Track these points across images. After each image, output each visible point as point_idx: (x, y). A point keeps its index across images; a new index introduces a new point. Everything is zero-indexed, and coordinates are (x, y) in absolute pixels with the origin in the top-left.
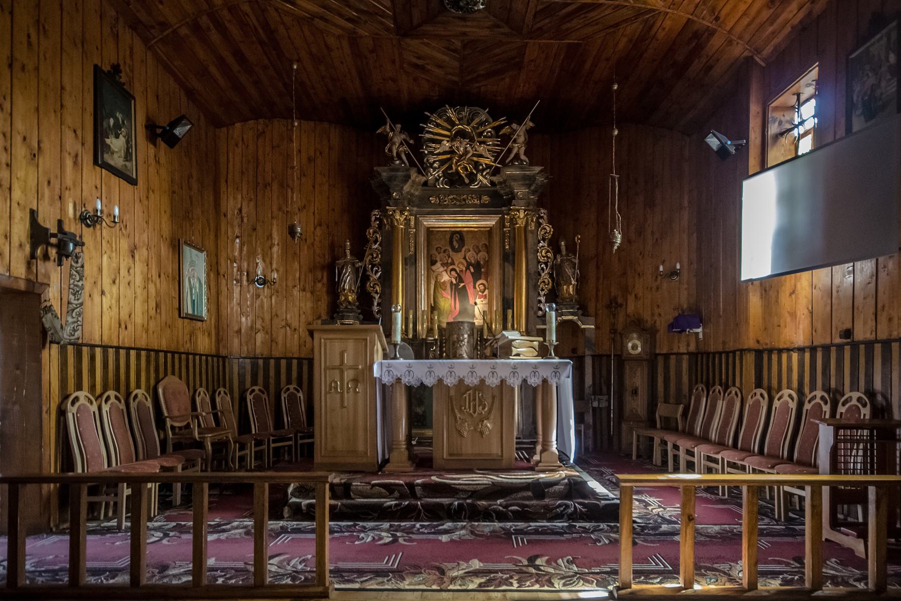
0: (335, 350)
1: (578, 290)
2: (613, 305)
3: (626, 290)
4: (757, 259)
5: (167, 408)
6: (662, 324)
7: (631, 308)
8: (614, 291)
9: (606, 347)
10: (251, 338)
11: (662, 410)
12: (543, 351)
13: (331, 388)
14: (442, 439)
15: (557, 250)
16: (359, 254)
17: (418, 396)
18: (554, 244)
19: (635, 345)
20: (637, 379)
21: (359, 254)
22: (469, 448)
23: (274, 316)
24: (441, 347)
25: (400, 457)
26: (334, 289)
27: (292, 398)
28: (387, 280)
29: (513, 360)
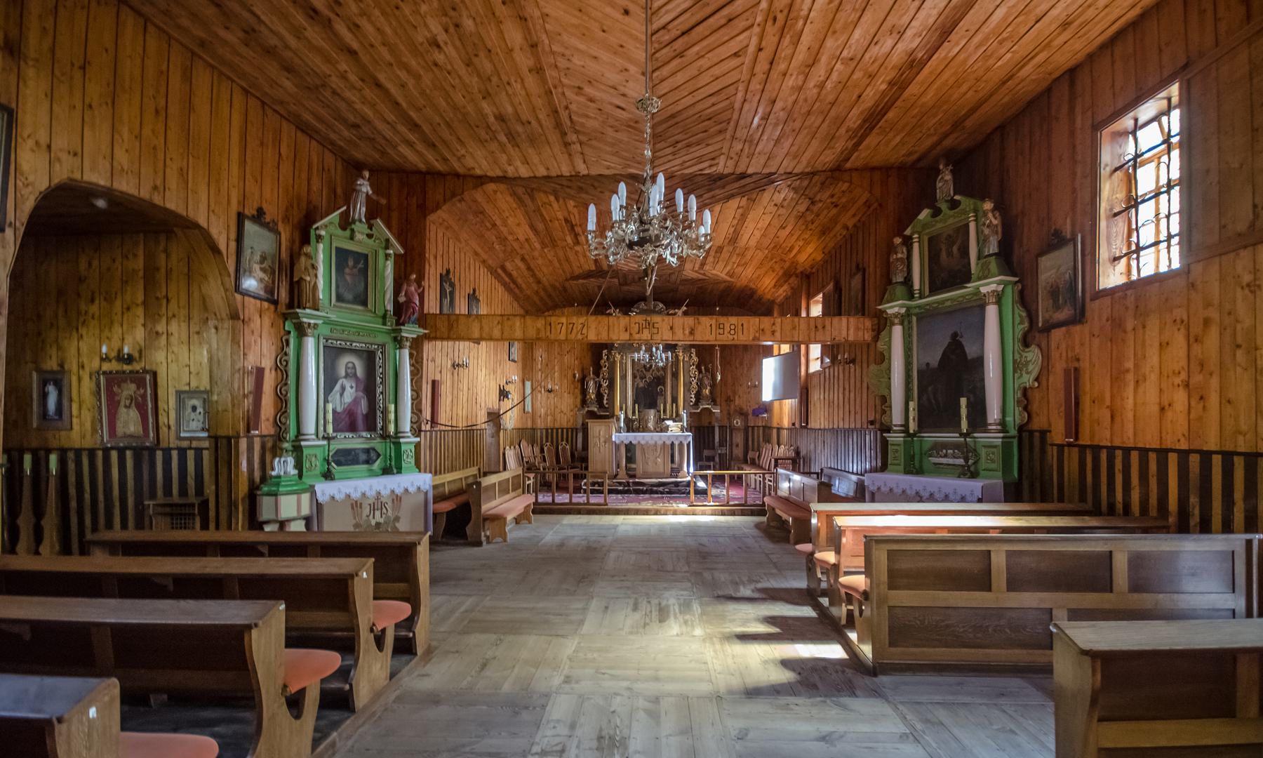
0: (596, 428)
1: (711, 392)
2: (729, 400)
3: (735, 393)
4: (767, 395)
5: (101, 412)
6: (750, 412)
7: (737, 402)
8: (730, 393)
9: (726, 423)
10: (546, 419)
11: (750, 455)
12: (682, 429)
13: (595, 445)
14: (639, 466)
15: (700, 372)
16: (597, 374)
17: (630, 448)
18: (698, 367)
19: (738, 422)
20: (739, 438)
21: (597, 374)
22: (651, 469)
23: (556, 407)
24: (619, 294)
25: (622, 472)
26: (584, 392)
27: (564, 449)
28: (611, 386)
29: (669, 433)
